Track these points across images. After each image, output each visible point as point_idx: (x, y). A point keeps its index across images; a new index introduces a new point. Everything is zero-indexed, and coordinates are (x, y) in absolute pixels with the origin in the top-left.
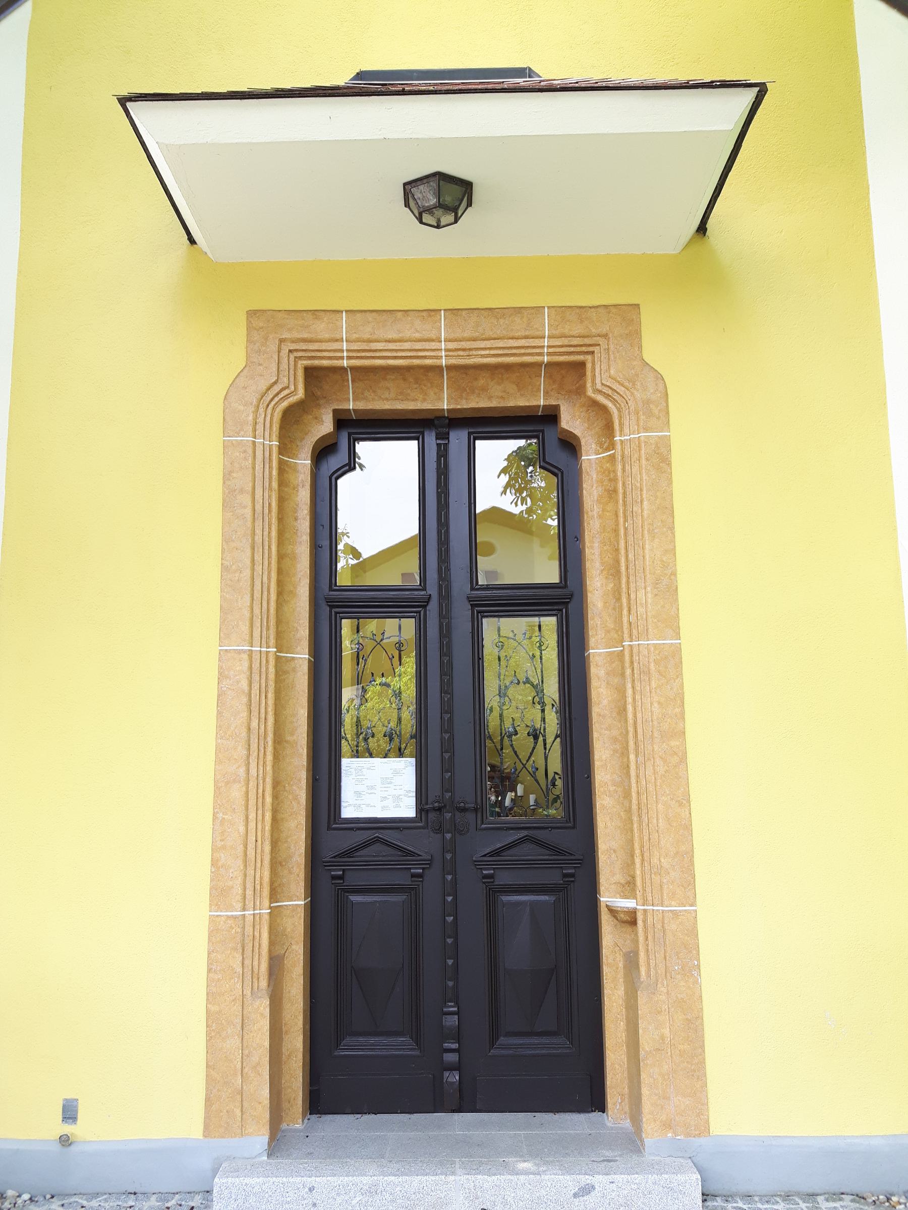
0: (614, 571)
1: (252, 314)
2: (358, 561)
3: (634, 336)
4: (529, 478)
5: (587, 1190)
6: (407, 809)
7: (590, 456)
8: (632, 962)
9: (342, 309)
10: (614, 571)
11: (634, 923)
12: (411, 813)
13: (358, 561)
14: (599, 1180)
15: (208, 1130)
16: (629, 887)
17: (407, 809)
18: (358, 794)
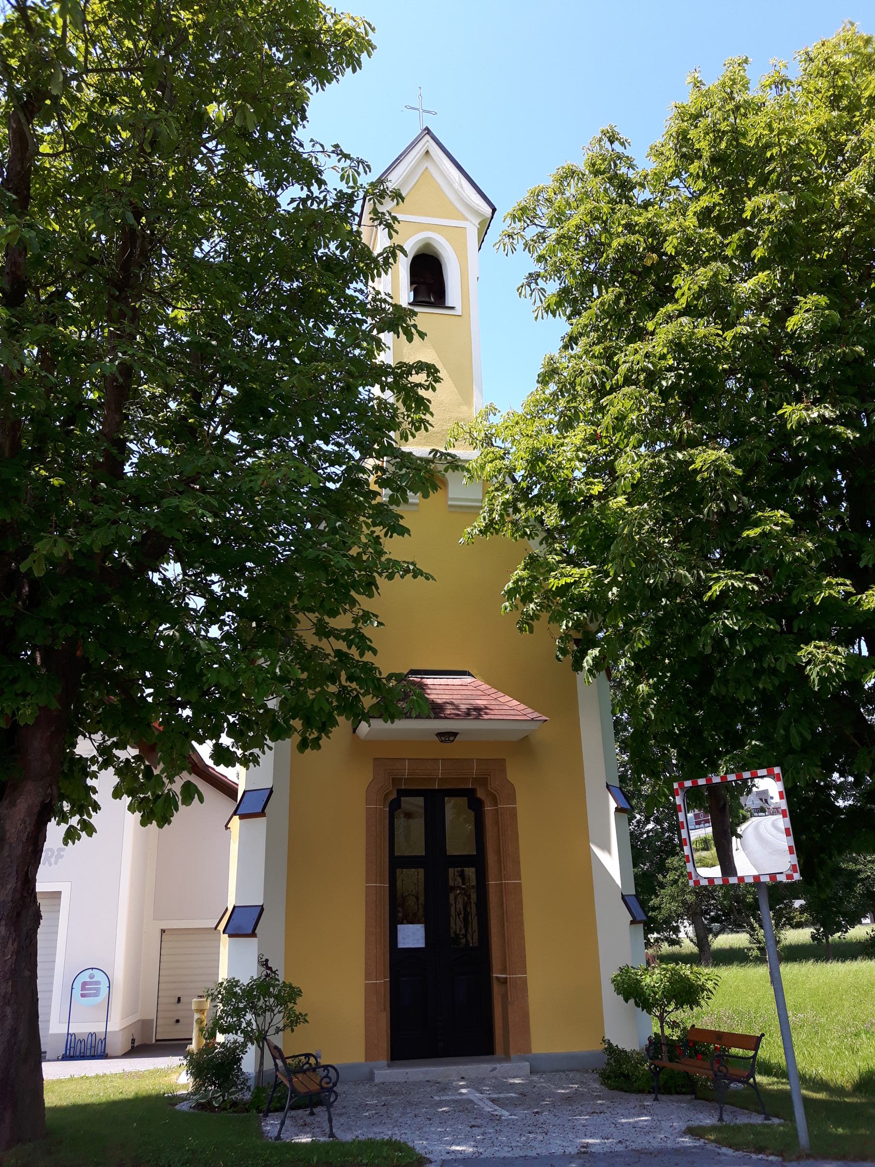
0: (498, 852)
1: (375, 759)
2: (210, 762)
3: (504, 771)
4: (77, 304)
5: (495, 1069)
6: (421, 944)
7: (488, 808)
8: (505, 996)
9: (405, 757)
10: (498, 852)
11: (506, 982)
12: (423, 945)
13: (210, 762)
14: (498, 1066)
15: (366, 1060)
16: (504, 970)
17: (421, 944)
18: (404, 938)
